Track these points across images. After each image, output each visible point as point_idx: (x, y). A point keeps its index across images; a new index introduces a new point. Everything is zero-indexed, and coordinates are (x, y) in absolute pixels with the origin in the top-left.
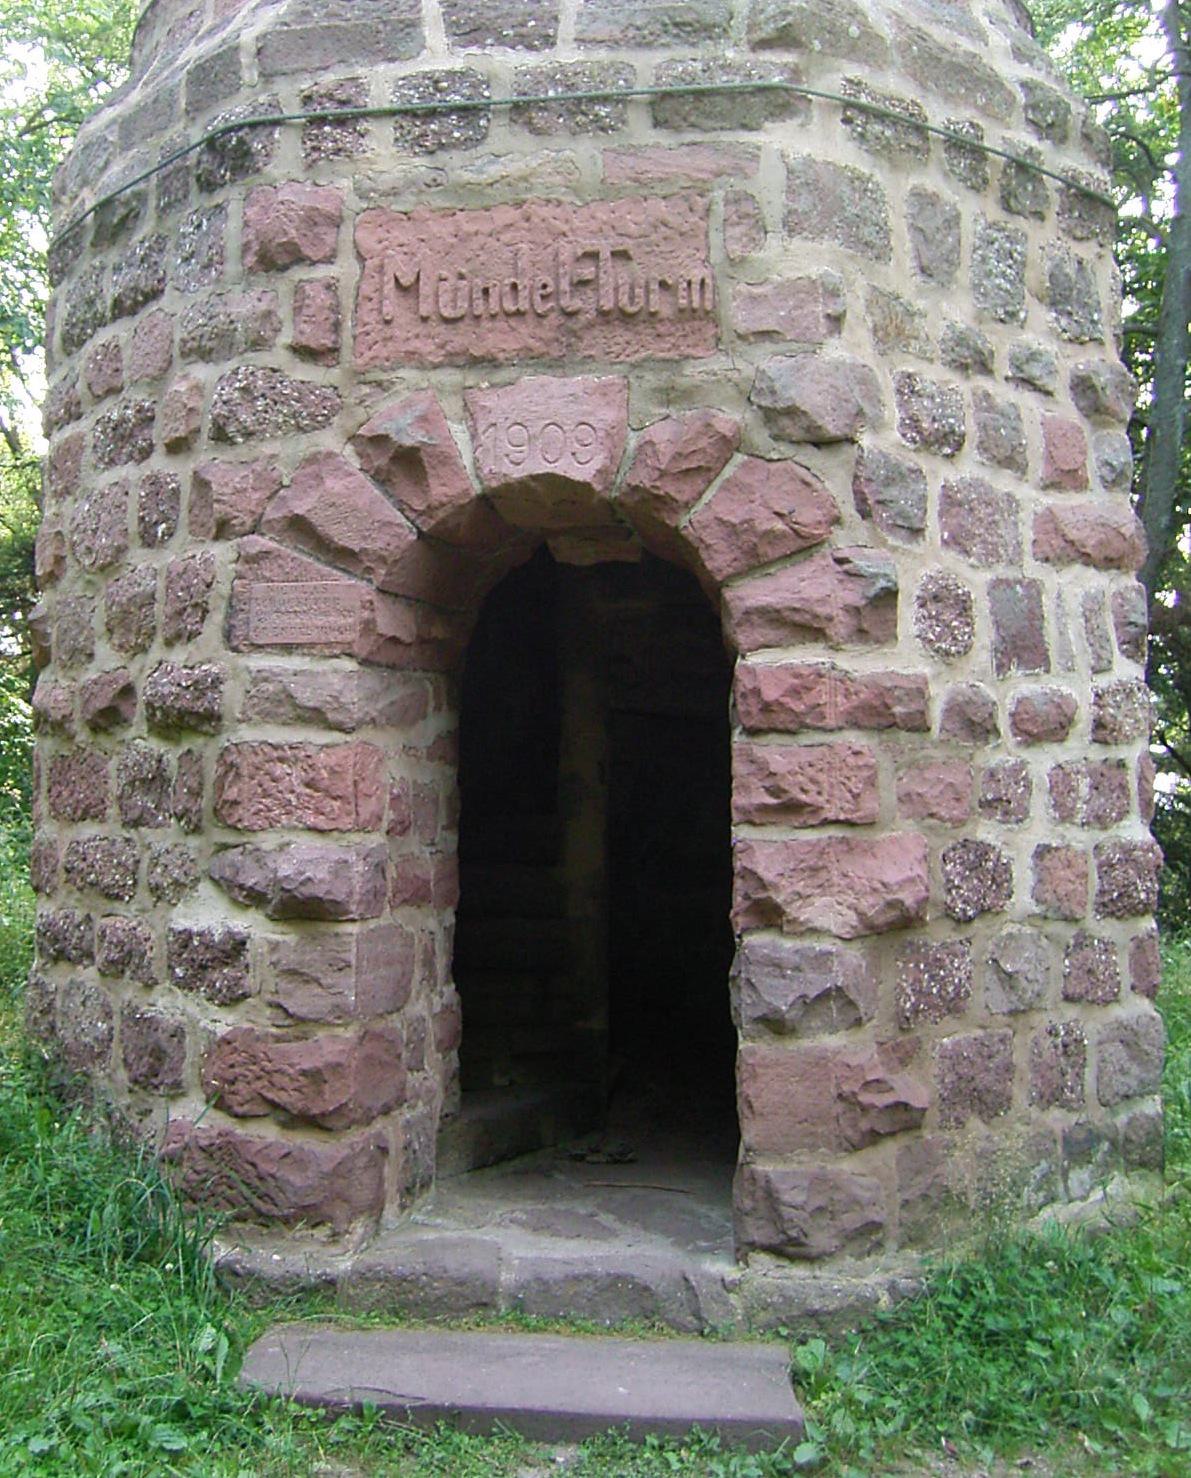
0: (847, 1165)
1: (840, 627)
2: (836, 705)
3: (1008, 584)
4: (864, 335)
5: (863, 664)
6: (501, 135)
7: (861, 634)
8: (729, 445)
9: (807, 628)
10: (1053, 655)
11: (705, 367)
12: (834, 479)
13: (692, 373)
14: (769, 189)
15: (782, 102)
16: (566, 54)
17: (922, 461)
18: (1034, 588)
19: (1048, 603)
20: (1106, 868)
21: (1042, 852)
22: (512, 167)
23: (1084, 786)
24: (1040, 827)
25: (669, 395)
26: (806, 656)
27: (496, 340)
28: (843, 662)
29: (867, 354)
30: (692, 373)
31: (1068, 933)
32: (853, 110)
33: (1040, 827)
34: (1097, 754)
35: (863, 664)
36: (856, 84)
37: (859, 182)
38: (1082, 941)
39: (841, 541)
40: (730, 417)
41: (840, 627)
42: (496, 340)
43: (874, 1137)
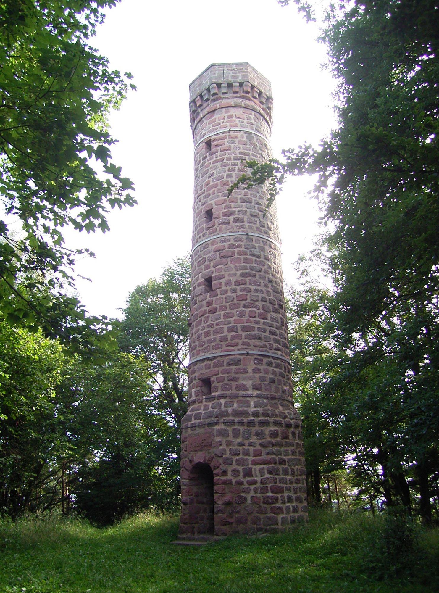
0: (222, 527)
1: (220, 475)
2: (220, 482)
3: (246, 468)
4: (225, 445)
5: (223, 478)
6: (197, 429)
7: (222, 475)
8: (213, 458)
9: (218, 475)
10: (254, 475)
11: (212, 450)
12: (221, 461)
13: (210, 451)
14: (215, 432)
15: (217, 423)
16: (202, 420)
17: (233, 457)
18: (251, 469)
19: (253, 470)
20: (264, 499)
21: (252, 497)
22: (198, 432)
23: (259, 490)
24: (252, 493)
25: (209, 453)
26: (218, 478)
27: (197, 449)
28: (221, 478)
29: (225, 447)
30: (210, 451)
31: (258, 506)
32: (225, 423)
33: (252, 493)
34: (262, 486)
35: (223, 478)
36: (225, 420)
37: (225, 430)
38: (260, 507)
39: (221, 466)
40: (213, 455)
41: (220, 475)
42: (197, 449)
43: (226, 525)
